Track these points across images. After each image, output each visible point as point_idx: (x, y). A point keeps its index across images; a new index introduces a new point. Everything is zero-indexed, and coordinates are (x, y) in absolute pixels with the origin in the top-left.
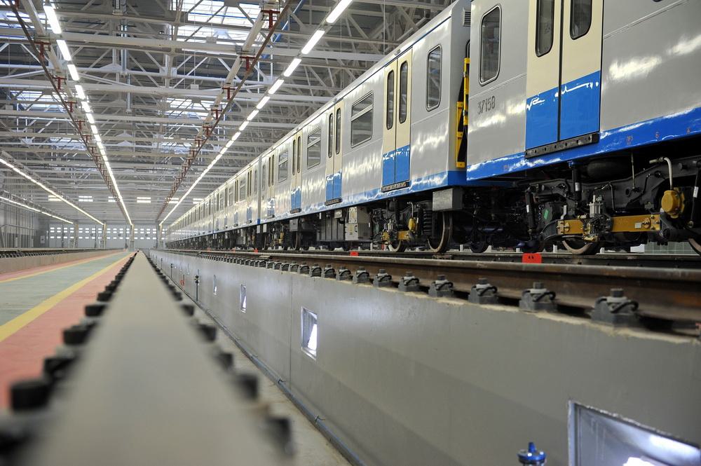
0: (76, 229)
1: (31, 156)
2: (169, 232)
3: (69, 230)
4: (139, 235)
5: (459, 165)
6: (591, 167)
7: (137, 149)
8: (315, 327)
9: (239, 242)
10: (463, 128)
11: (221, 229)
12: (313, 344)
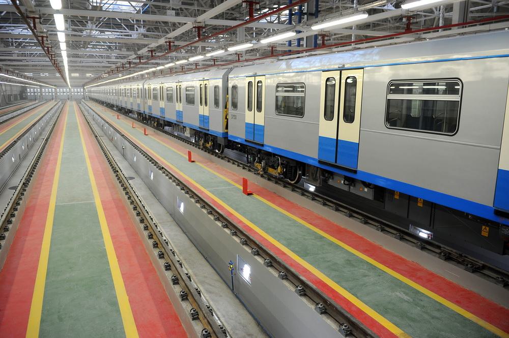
0: (41, 90)
3: (37, 90)
4: (74, 92)
5: (226, 131)
12: (182, 209)
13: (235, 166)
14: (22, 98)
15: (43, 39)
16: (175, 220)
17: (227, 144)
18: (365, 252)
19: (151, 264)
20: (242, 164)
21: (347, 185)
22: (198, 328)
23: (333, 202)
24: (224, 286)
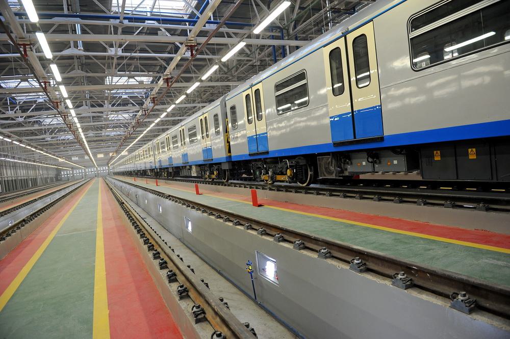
0: (73, 172)
1: (51, 145)
2: (113, 168)
3: (70, 172)
4: (101, 171)
5: (229, 154)
6: (268, 160)
7: (96, 136)
8: (190, 222)
9: (147, 174)
10: (229, 142)
11: (139, 169)
12: (190, 228)
13: (243, 189)
14: (57, 180)
15: (57, 104)
16: (184, 244)
17: (231, 168)
18: (411, 230)
19: (147, 272)
20: (248, 185)
21: (371, 162)
22: (204, 335)
23: (355, 191)
24: (244, 298)
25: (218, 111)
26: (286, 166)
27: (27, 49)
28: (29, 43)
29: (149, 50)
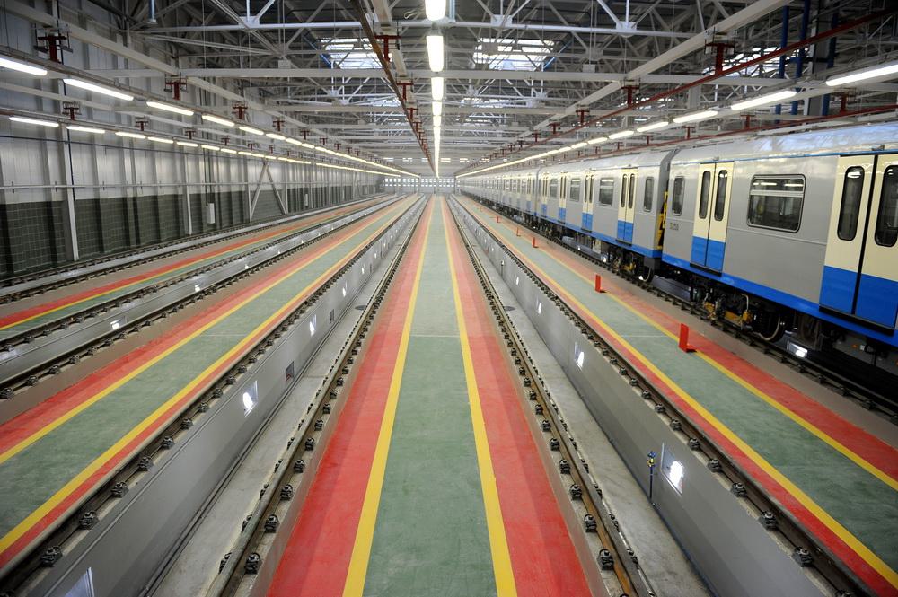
0: (402, 180)
5: (659, 248)
13: (669, 305)
14: (378, 191)
20: (680, 301)
24: (637, 490)
25: (655, 173)
26: (743, 304)
27: (390, 46)
28: (395, 34)
29: (563, 20)
